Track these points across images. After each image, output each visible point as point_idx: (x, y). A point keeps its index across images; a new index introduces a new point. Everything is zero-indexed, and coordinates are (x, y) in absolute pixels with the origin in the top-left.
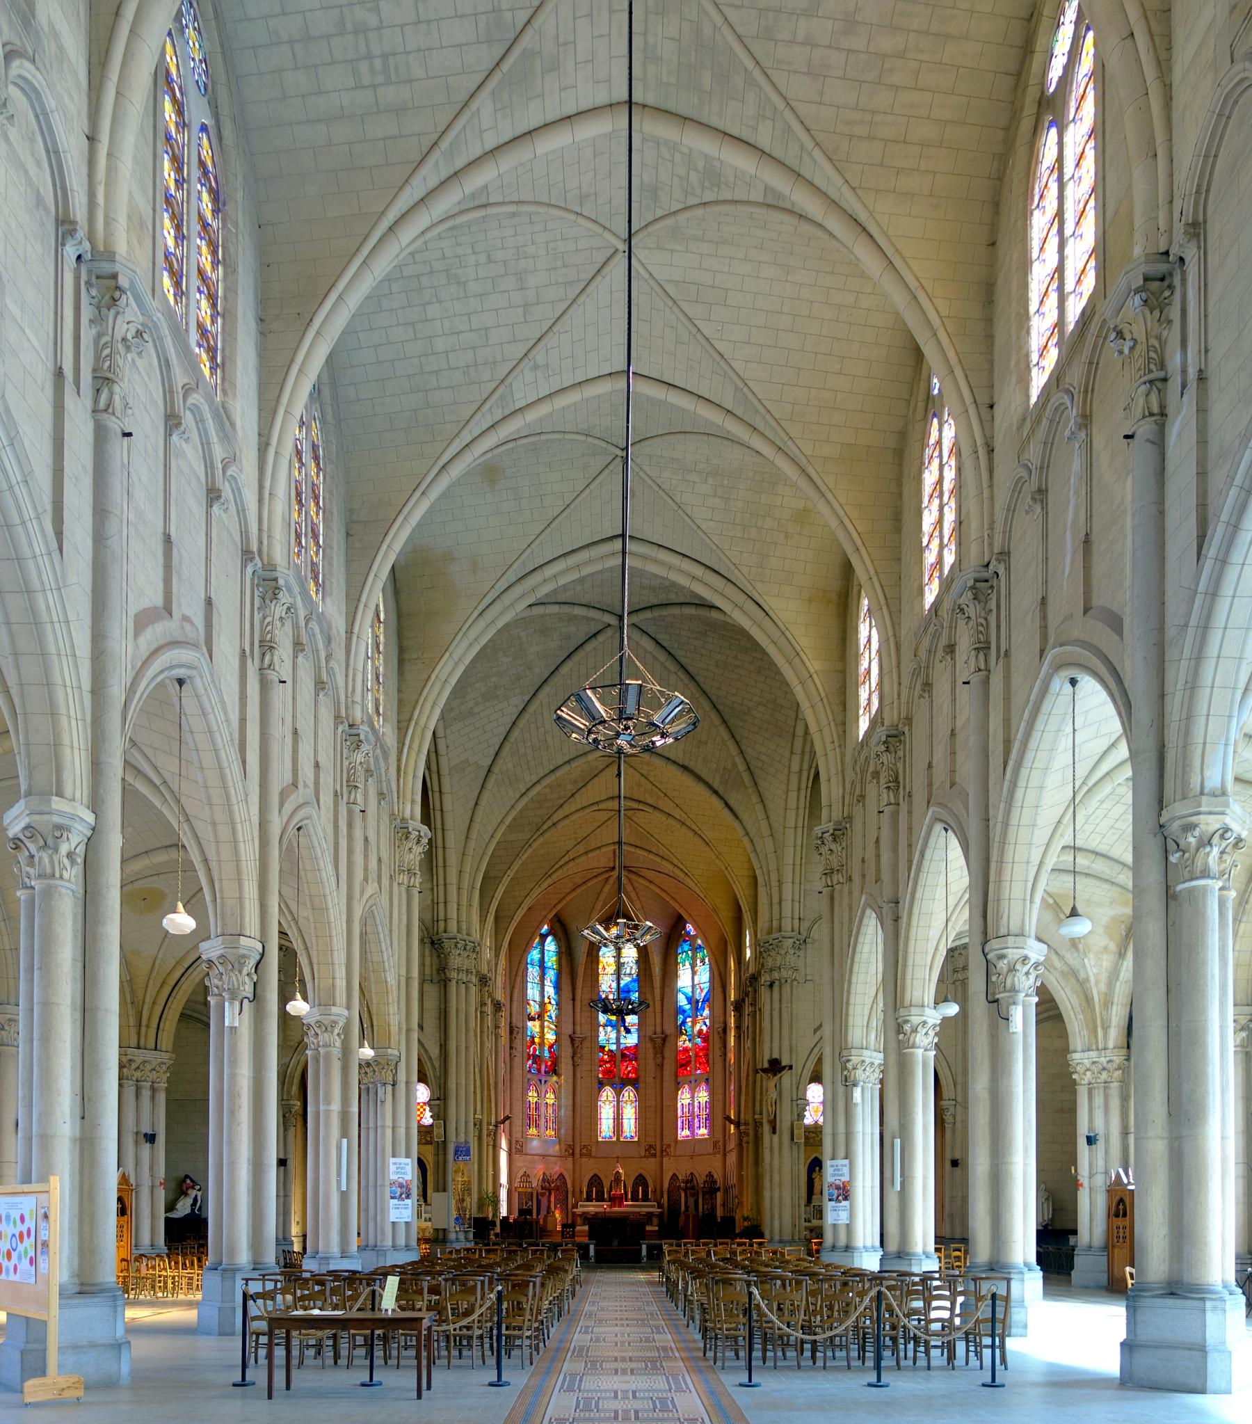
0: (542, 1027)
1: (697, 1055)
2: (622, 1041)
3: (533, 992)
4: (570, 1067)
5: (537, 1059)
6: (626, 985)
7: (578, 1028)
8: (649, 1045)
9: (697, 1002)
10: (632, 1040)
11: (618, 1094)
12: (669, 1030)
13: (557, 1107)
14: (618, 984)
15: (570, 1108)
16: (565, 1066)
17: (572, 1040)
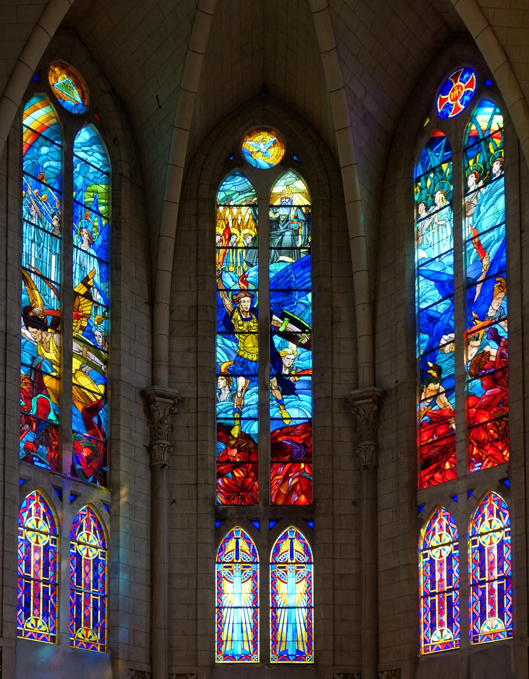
0: (66, 354)
1: (472, 425)
2: (274, 412)
3: (37, 251)
4: (143, 470)
5: (51, 434)
6: (282, 275)
7: (163, 374)
8: (341, 421)
9: (471, 284)
10: (298, 409)
11: (265, 546)
12: (393, 373)
13: (107, 569)
14: (263, 270)
15: (143, 576)
16: (130, 465)
17: (147, 398)
